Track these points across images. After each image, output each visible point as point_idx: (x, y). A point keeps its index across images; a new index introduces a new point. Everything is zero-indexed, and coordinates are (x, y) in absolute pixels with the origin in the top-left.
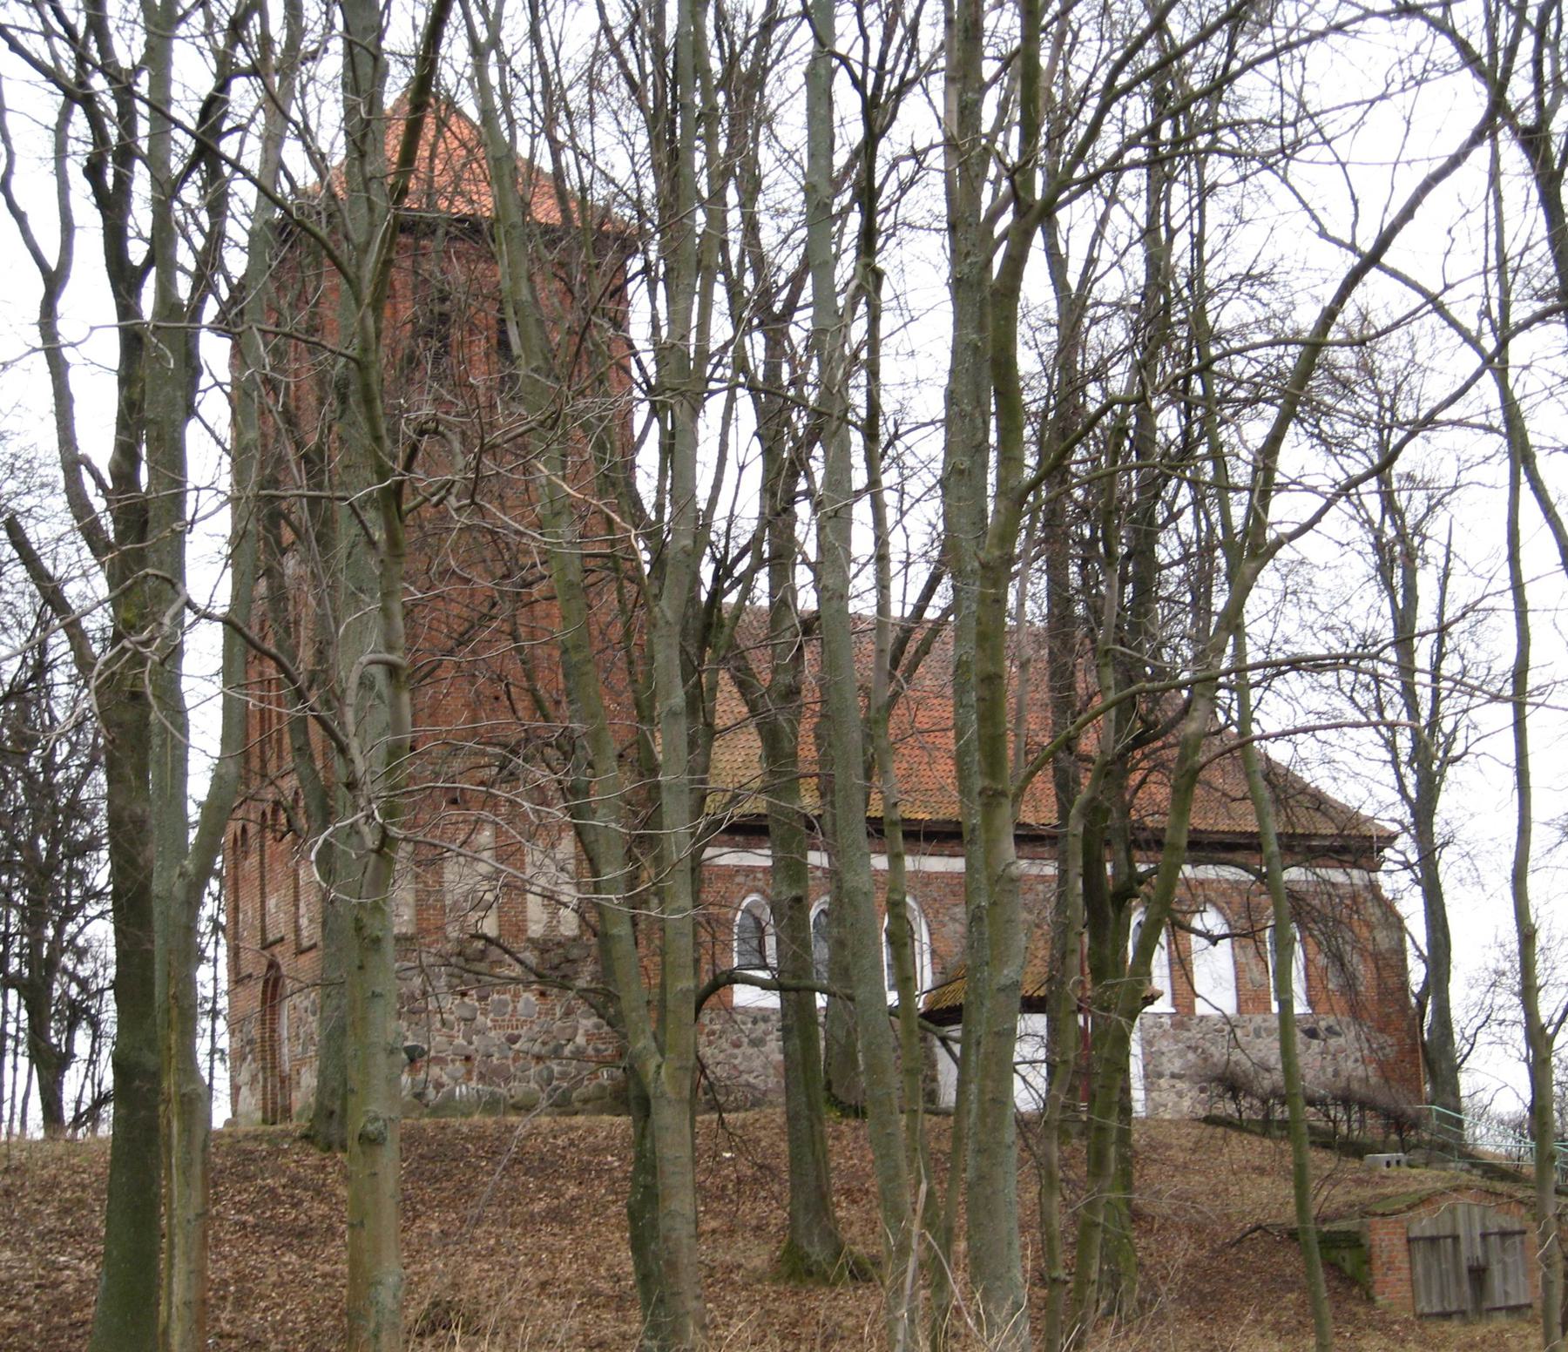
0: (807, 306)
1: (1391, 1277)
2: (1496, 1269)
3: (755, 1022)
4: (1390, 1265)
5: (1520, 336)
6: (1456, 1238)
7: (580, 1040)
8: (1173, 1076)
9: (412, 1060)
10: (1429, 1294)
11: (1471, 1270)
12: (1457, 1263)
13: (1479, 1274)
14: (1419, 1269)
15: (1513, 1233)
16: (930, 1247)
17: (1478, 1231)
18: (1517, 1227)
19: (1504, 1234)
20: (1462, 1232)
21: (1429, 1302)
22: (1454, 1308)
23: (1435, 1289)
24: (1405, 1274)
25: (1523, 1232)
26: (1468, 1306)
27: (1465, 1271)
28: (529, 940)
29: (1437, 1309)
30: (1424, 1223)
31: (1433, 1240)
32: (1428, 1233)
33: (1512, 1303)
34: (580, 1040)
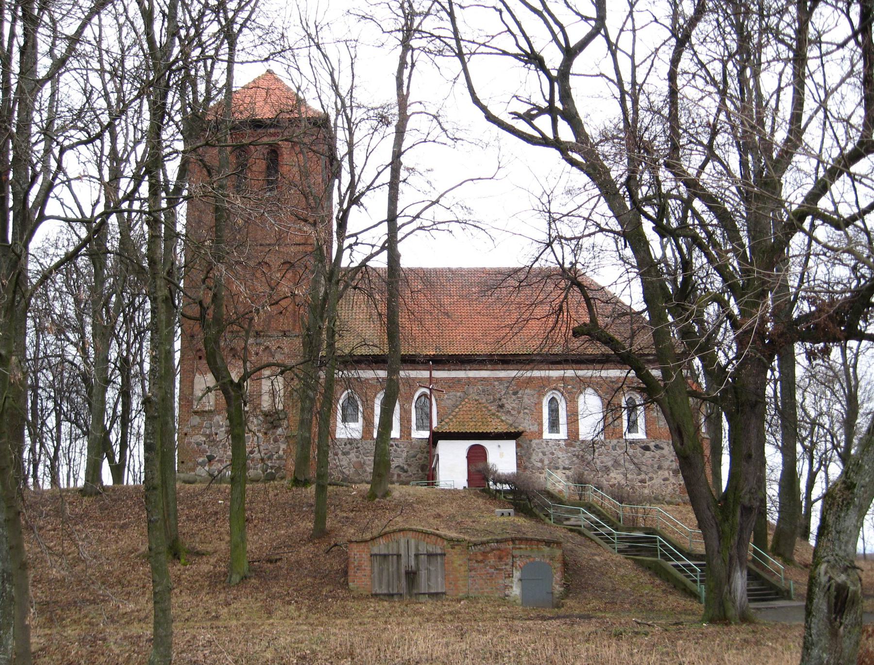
0: (858, 61)
1: (359, 574)
2: (423, 573)
3: (345, 445)
4: (359, 568)
5: (560, 136)
6: (399, 556)
7: (281, 452)
8: (564, 468)
9: (210, 461)
10: (380, 583)
11: (407, 573)
12: (398, 569)
13: (412, 576)
14: (376, 570)
15: (436, 555)
16: (632, 559)
17: (413, 552)
18: (439, 551)
19: (430, 555)
20: (402, 552)
21: (380, 587)
22: (395, 591)
23: (385, 581)
24: (368, 572)
25: (443, 555)
26: (404, 591)
27: (403, 571)
28: (261, 411)
29: (385, 592)
30: (381, 547)
31: (385, 556)
32: (382, 552)
33: (432, 591)
34: (281, 452)
